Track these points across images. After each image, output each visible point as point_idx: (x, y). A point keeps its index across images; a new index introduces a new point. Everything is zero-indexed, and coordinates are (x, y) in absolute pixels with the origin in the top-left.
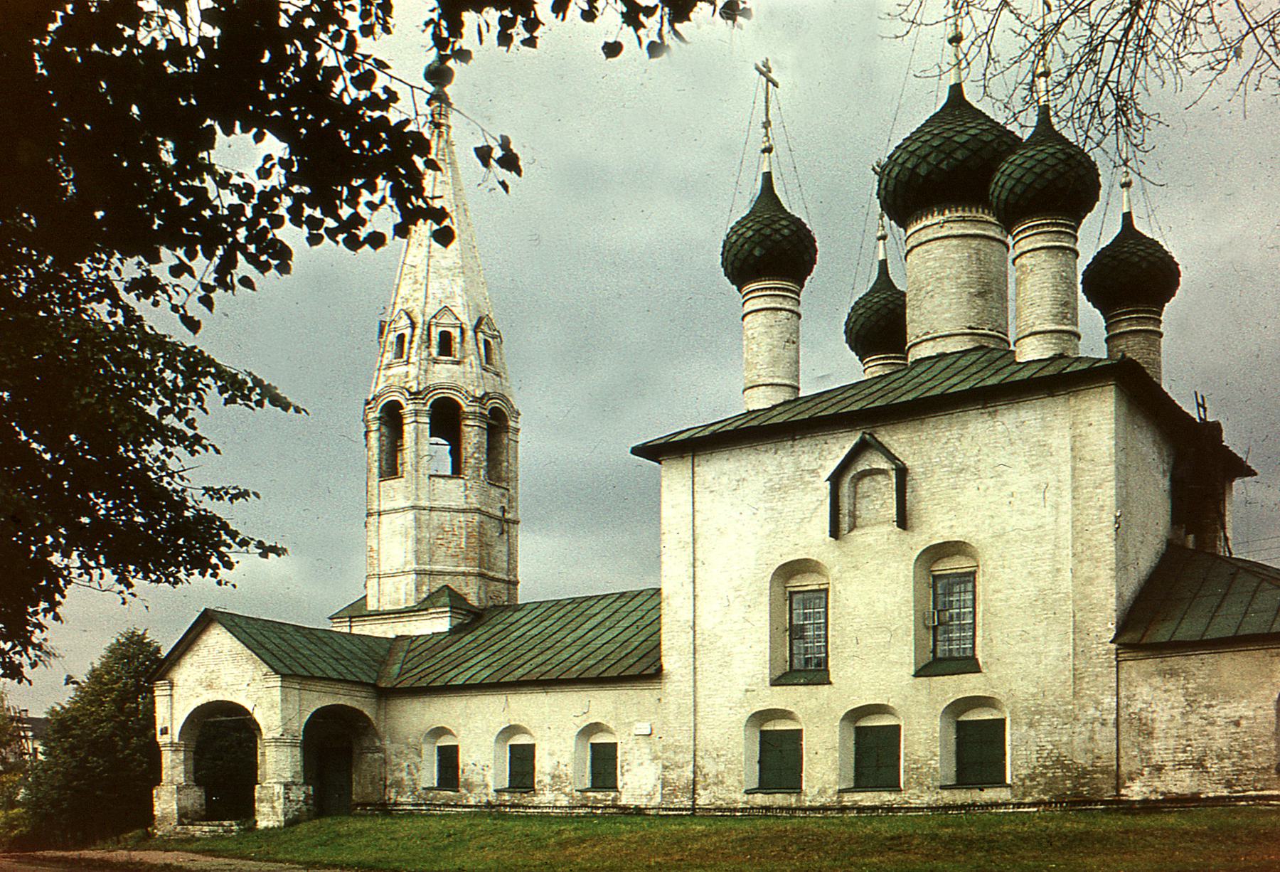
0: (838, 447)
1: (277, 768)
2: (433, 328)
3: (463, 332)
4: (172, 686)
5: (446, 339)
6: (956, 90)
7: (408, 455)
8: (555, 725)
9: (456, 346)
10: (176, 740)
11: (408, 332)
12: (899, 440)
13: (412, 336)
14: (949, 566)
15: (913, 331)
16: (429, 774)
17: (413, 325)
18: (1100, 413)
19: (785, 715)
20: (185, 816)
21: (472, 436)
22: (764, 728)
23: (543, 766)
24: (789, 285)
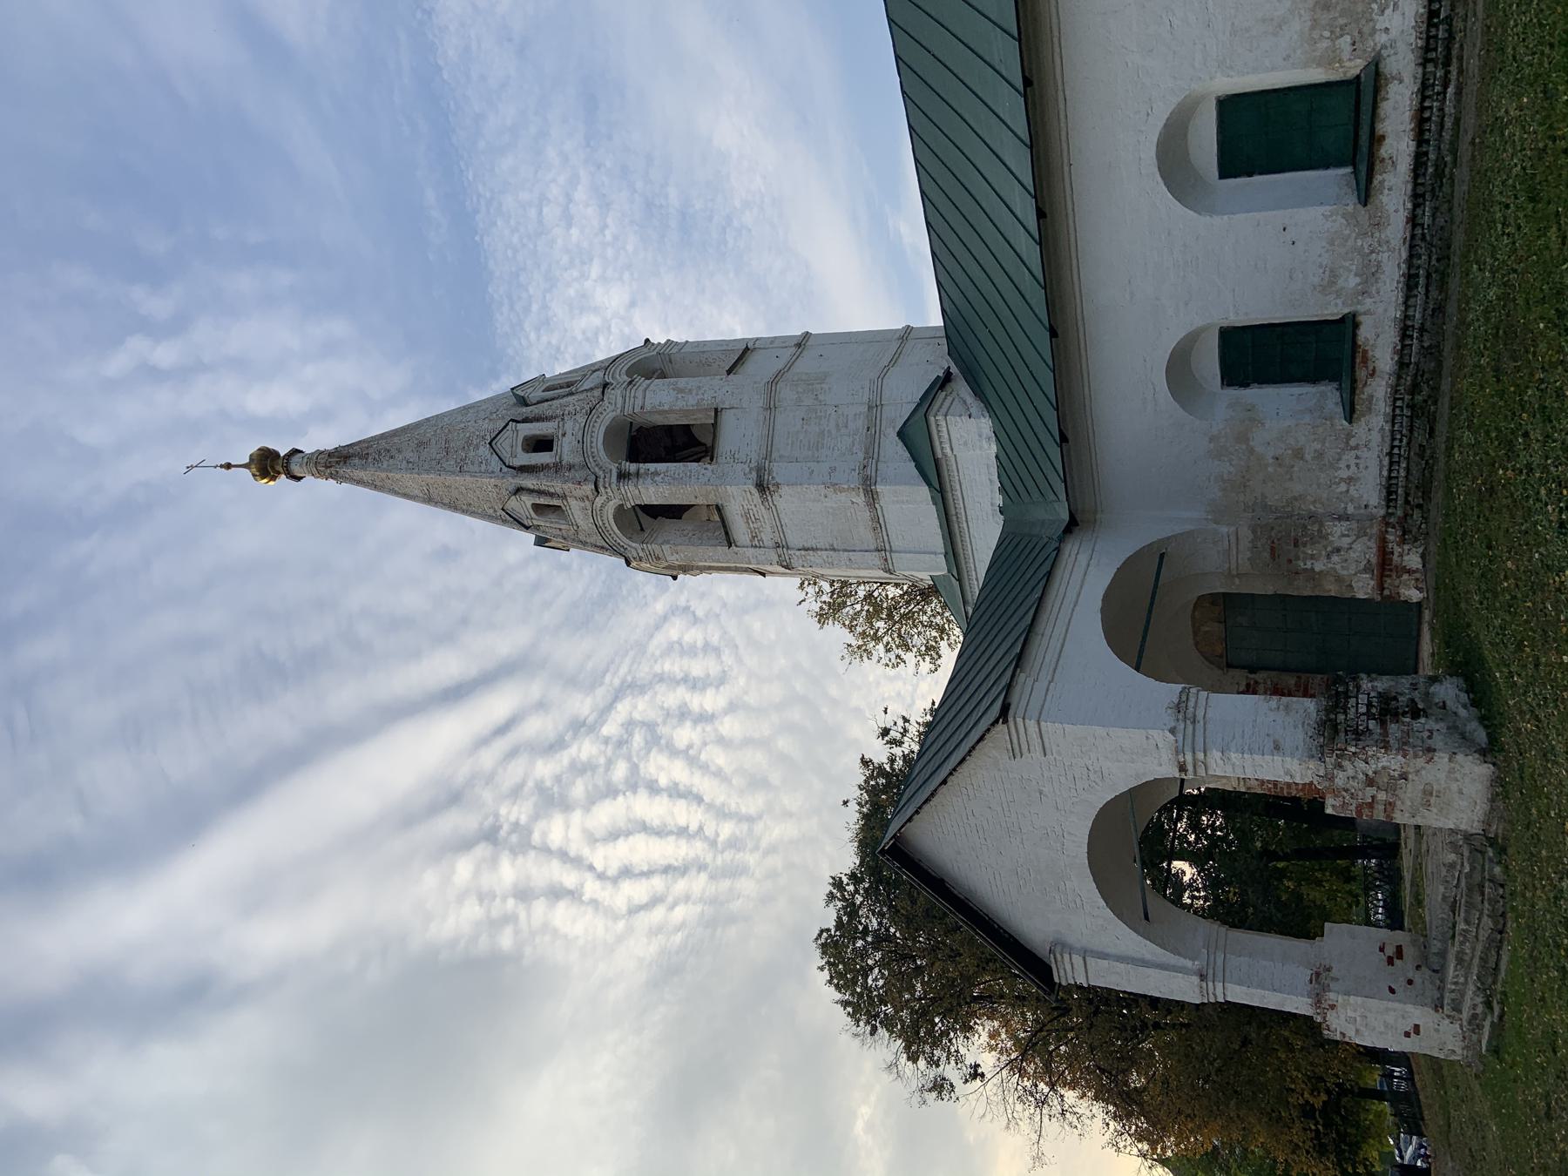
1: (1258, 744)
2: (517, 463)
9: (555, 502)
11: (528, 500)
16: (1287, 410)
20: (1421, 968)
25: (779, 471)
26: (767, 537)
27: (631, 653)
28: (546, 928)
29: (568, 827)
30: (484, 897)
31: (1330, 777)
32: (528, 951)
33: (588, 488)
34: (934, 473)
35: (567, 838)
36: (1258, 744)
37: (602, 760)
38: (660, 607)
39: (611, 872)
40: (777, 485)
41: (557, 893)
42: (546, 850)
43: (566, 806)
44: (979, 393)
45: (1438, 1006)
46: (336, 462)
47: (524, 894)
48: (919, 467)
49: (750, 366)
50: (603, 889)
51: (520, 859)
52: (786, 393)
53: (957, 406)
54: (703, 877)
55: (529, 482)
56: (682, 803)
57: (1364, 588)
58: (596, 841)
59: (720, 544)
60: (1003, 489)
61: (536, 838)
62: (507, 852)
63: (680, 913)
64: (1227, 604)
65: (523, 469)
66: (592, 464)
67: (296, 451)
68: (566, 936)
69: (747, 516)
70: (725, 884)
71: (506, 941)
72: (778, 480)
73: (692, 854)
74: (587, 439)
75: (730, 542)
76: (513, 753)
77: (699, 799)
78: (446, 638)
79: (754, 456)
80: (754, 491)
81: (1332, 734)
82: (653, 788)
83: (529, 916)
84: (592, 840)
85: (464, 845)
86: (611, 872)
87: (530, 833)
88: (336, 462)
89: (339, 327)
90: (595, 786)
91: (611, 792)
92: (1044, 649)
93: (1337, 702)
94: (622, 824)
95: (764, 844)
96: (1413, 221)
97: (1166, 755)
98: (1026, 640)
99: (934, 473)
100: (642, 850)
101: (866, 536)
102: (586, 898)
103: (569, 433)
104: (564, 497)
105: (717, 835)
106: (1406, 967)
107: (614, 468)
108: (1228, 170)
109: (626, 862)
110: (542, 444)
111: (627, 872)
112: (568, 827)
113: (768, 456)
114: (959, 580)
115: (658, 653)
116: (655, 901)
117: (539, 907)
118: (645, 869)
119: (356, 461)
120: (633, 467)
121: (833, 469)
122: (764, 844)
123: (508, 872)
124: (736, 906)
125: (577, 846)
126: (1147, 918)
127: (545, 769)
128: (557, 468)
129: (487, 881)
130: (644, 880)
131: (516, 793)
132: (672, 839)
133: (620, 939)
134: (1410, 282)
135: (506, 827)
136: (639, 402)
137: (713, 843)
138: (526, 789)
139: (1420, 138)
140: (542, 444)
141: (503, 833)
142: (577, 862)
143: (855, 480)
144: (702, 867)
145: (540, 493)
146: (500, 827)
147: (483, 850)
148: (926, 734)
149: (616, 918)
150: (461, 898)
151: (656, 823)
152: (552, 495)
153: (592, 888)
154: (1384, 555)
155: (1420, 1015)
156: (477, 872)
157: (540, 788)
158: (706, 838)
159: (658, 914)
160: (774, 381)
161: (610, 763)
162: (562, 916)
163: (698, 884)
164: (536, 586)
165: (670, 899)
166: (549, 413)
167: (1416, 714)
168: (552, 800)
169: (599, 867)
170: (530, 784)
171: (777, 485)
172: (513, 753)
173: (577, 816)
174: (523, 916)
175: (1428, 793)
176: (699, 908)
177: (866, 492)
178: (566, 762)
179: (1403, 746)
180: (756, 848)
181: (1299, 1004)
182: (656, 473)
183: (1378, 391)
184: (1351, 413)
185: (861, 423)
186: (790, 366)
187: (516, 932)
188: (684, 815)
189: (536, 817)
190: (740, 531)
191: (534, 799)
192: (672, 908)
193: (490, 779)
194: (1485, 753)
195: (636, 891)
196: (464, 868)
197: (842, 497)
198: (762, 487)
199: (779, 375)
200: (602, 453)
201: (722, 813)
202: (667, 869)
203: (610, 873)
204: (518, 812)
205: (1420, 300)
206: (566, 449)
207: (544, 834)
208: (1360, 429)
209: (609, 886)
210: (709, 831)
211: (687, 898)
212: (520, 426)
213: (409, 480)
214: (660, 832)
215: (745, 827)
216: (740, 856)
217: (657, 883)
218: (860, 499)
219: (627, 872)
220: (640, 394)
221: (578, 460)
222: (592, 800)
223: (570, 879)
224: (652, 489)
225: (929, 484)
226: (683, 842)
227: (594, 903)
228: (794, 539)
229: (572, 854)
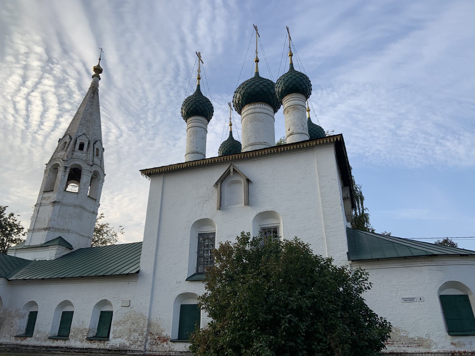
3: (89, 143)
6: (257, 73)
9: (65, 148)
11: (68, 141)
16: (22, 324)
23: (75, 323)
24: (203, 119)
25: (58, 207)
26: (44, 201)
27: (109, 116)
28: (12, 73)
29: (50, 86)
30: (27, 54)
32: (5, 65)
33: (65, 159)
34: (46, 245)
35: (45, 85)
37: (72, 101)
38: (123, 127)
39: (30, 98)
40: (54, 206)
41: (25, 79)
42: (41, 78)
43: (57, 87)
44: (64, 256)
46: (94, 90)
47: (26, 68)
48: (50, 241)
50: (24, 94)
51: (39, 68)
52: (78, 210)
54: (23, 128)
55: (72, 143)
56: (52, 125)
58: (42, 94)
59: (45, 189)
60: (39, 261)
61: (47, 75)
62: (43, 65)
63: (11, 118)
65: (76, 141)
66: (71, 160)
67: (100, 79)
68: (8, 78)
69: (49, 197)
70: (19, 134)
71: (9, 58)
72: (55, 207)
73: (33, 125)
74: (78, 160)
76: (79, 73)
77: (53, 130)
78: (122, 60)
79: (63, 201)
80: (53, 201)
82: (59, 116)
83: (17, 68)
84: (43, 93)
85: (48, 50)
86: (30, 98)
87: (50, 74)
88: (94, 90)
89: (220, 50)
90: (63, 97)
91: (60, 102)
94: (47, 104)
95: (33, 149)
96: (44, 347)
99: (46, 245)
100: (36, 109)
101: (38, 226)
102: (22, 88)
103: (82, 155)
104: (66, 151)
105: (39, 135)
107: (69, 166)
108: (182, 306)
109: (33, 103)
110: (81, 147)
111: (29, 103)
112: (50, 86)
113: (62, 204)
114: (22, 248)
115: (108, 125)
116: (16, 110)
117: (20, 72)
118: (29, 109)
119: (92, 95)
120: (68, 170)
121: (55, 220)
122: (33, 149)
123: (35, 64)
124: (11, 137)
125: (41, 88)
127: (72, 83)
128: (73, 151)
129: (33, 56)
130: (25, 108)
131: (64, 71)
132: (40, 119)
133: (4, 97)
134: (34, 347)
135: (52, 66)
136: (85, 174)
137: (35, 133)
138: (66, 75)
139: (56, 347)
140: (81, 147)
141: (50, 65)
142: (35, 87)
143: (50, 226)
144: (27, 128)
145: (69, 145)
146: (53, 64)
147: (45, 57)
149: (12, 96)
150: (28, 47)
151: (46, 115)
152: (67, 148)
153: (25, 90)
156: (36, 53)
157: (65, 80)
158: (38, 130)
159: (11, 111)
160: (81, 207)
161: (71, 104)
162: (16, 78)
163: (21, 125)
164: (135, 91)
165: (17, 116)
166: (89, 150)
168: (60, 83)
169: (33, 94)
170: (67, 77)
171: (54, 206)
172: (79, 73)
173: (53, 90)
174: (18, 66)
176: (11, 125)
177: (47, 228)
178: (73, 89)
180: (32, 147)
182: (65, 176)
183: (19, 342)
184: (16, 336)
186: (88, 211)
187: (12, 62)
188: (48, 125)
189: (54, 76)
190: (47, 195)
191: (62, 77)
192: (13, 116)
193: (71, 64)
195: (22, 105)
196: (39, 49)
197: (47, 222)
198: (54, 202)
199: (84, 208)
200: (73, 163)
201: (47, 136)
202: (28, 116)
203: (29, 97)
204: (57, 70)
206: (78, 153)
207: (48, 78)
208: (13, 338)
209: (24, 96)
210: (40, 132)
211: (16, 121)
212: (87, 142)
213: (83, 109)
214: (42, 116)
215: (40, 144)
216: (30, 141)
217: (24, 112)
218: (46, 227)
219: (29, 103)
220: (87, 174)
221: (74, 156)
222: (58, 96)
223: (30, 83)
224: (61, 175)
225: (45, 243)
226: (38, 123)
227: (19, 90)
228: (41, 208)
229: (38, 86)
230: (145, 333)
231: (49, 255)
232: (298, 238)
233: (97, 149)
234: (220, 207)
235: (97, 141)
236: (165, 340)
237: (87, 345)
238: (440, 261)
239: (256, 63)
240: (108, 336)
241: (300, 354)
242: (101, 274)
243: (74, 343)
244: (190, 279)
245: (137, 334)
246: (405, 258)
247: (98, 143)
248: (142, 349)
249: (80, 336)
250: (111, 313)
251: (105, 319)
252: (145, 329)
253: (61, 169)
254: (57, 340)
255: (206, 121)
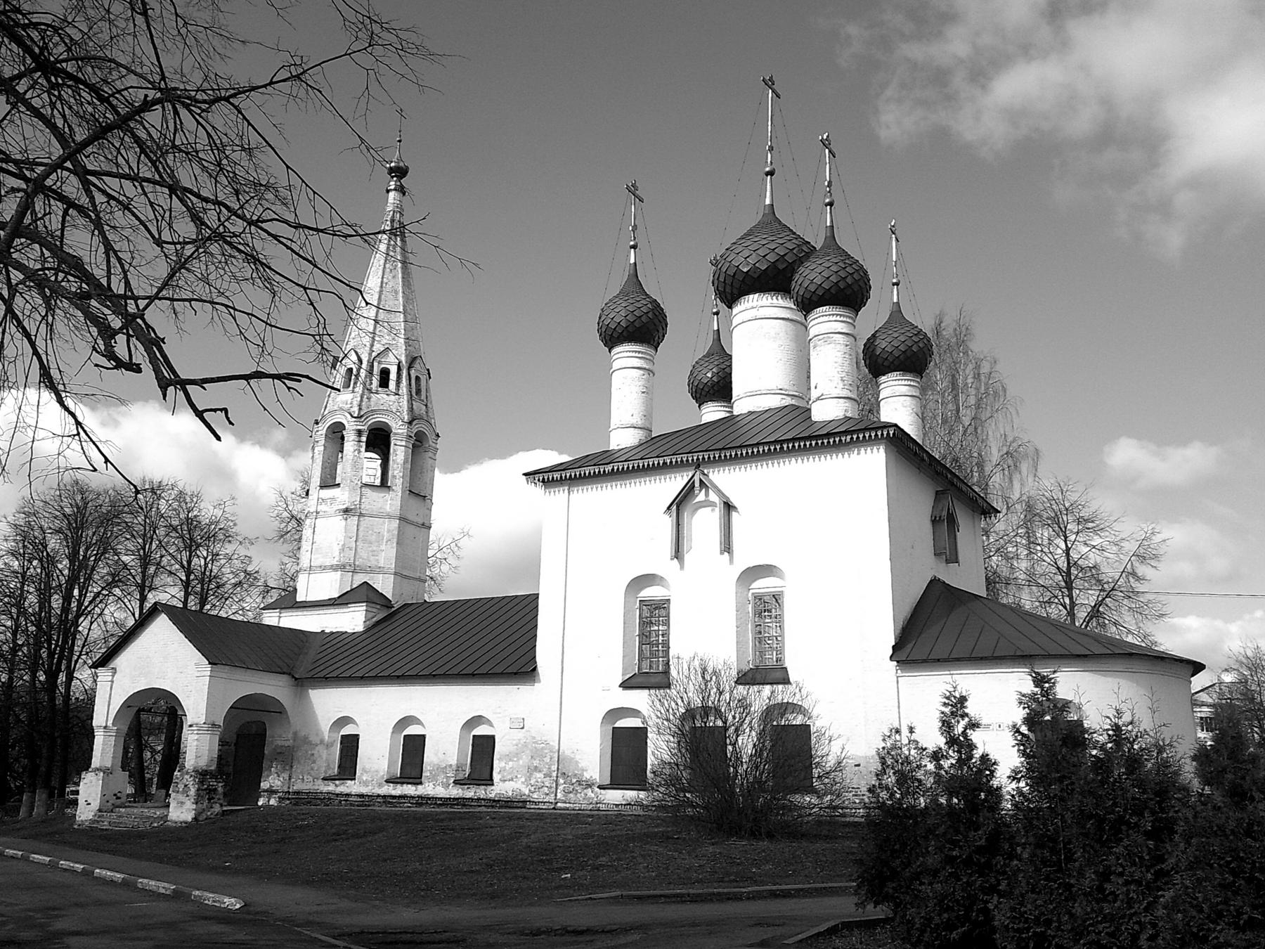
0: (673, 484)
1: (198, 748)
2: (376, 364)
3: (399, 369)
4: (114, 670)
5: (385, 374)
7: (344, 470)
8: (445, 713)
9: (392, 385)
10: (110, 723)
12: (727, 479)
13: (358, 371)
14: (763, 585)
15: (736, 392)
17: (360, 361)
18: (871, 463)
19: (634, 713)
20: (112, 803)
21: (399, 453)
22: (617, 725)
23: (431, 756)
31: (187, 773)
36: (198, 748)
44: (378, 623)
45: (100, 810)
49: (414, 502)
53: (371, 615)
54: (832, 341)
55: (363, 373)
57: (264, 785)
60: (332, 633)
64: (263, 736)
65: (372, 366)
69: (333, 499)
75: (322, 487)
81: (202, 775)
92: (239, 674)
93: (212, 775)
96: (379, 796)
97: (196, 721)
98: (1085, 656)
106: (113, 800)
110: (384, 382)
120: (364, 439)
126: (231, 423)
134: (362, 796)
139: (400, 797)
148: (1012, 609)
152: (355, 383)
154: (275, 792)
155: (95, 805)
167: (209, 799)
175: (182, 803)
179: (198, 795)
181: (96, 762)
183: (331, 787)
184: (324, 779)
185: (373, 563)
194: (195, 819)
198: (346, 511)
205: (485, 809)
206: (383, 399)
230: (554, 774)
231: (353, 620)
232: (972, 708)
233: (417, 378)
234: (678, 554)
235: (414, 359)
236: (589, 785)
237: (456, 792)
238: (1137, 665)
239: (668, 522)
240: (491, 779)
241: (1262, 814)
242: (398, 673)
243: (428, 789)
244: (626, 685)
245: (539, 775)
246: (982, 659)
247: (417, 365)
248: (551, 798)
249: (441, 778)
250: (490, 740)
251: (483, 748)
252: (554, 767)
253: (350, 437)
254: (402, 783)
255: (651, 351)
